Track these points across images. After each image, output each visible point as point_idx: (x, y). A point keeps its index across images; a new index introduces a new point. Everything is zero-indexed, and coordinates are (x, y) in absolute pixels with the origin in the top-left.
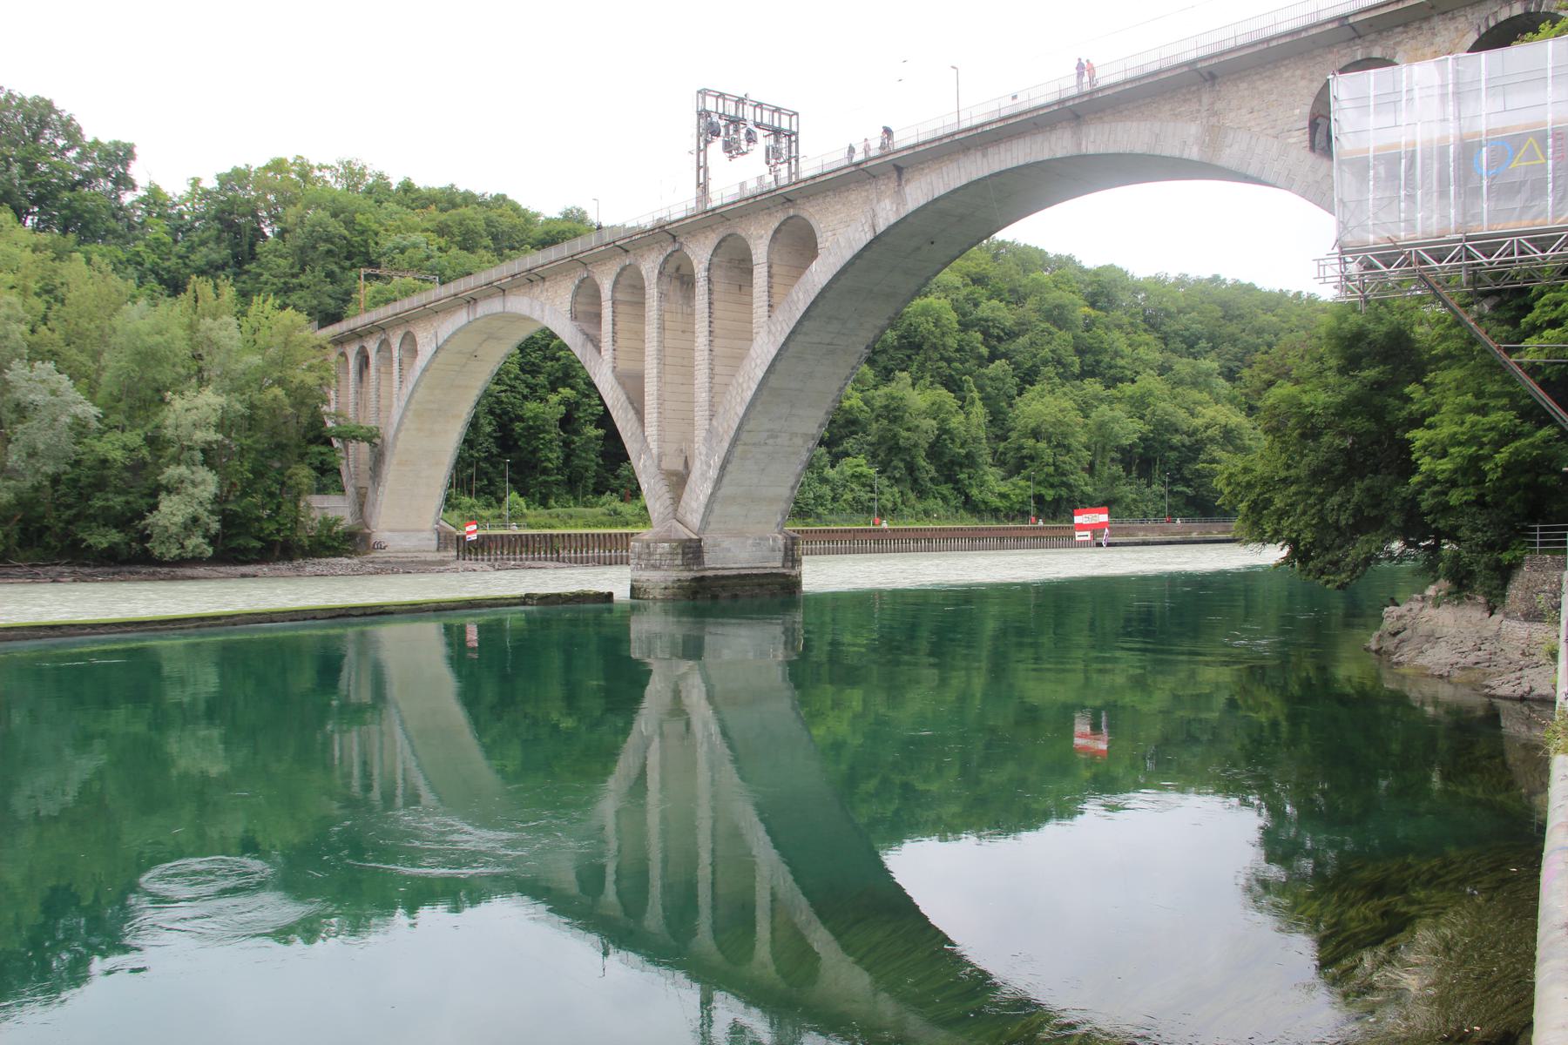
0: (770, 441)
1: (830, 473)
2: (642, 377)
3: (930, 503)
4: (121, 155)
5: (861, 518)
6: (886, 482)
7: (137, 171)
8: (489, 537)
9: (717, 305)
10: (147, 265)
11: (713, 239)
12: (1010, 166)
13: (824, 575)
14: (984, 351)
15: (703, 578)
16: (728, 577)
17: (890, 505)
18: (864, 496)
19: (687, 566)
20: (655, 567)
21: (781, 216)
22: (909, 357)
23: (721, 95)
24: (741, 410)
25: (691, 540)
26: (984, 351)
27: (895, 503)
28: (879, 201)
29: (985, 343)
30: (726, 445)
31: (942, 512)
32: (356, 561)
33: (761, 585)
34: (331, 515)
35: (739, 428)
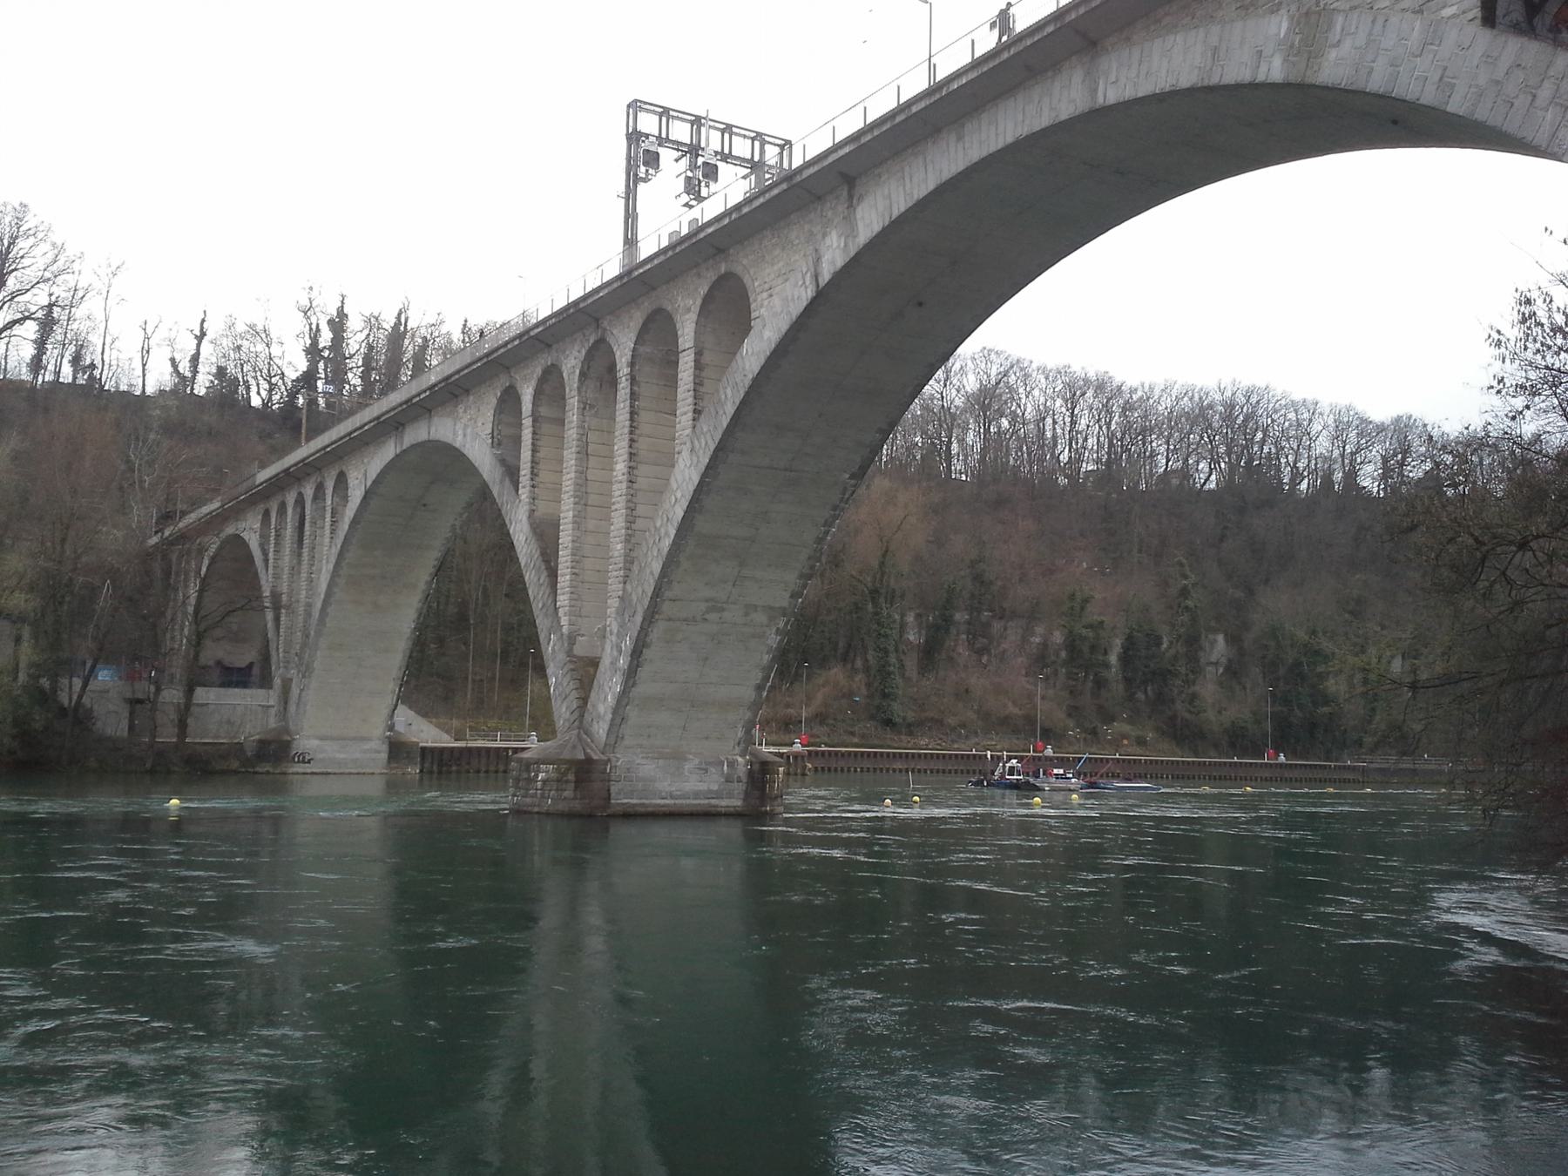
0: (713, 616)
8: (470, 749)
9: (644, 417)
11: (636, 319)
21: (711, 276)
23: (665, 113)
24: (657, 567)
28: (824, 235)
30: (639, 619)
35: (657, 593)
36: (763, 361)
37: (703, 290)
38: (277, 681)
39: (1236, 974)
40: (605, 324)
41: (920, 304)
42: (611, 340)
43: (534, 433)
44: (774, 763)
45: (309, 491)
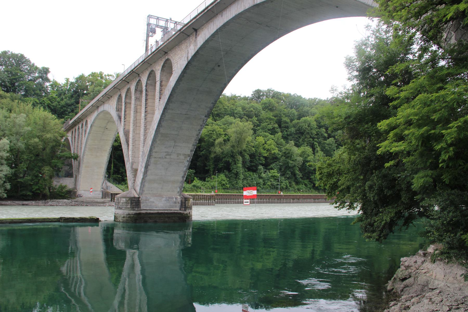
0: (167, 157)
1: (263, 175)
2: (129, 132)
3: (300, 186)
4: (46, 71)
5: (274, 191)
6: (283, 178)
7: (50, 76)
10: (46, 104)
12: (230, 18)
13: (201, 214)
14: (326, 135)
15: (140, 214)
16: (153, 214)
17: (284, 187)
18: (275, 183)
19: (132, 208)
20: (120, 208)
21: (164, 60)
22: (300, 137)
23: (158, 18)
24: (150, 143)
25: (135, 197)
26: (326, 135)
27: (287, 186)
28: (190, 46)
29: (327, 132)
30: (146, 158)
31: (304, 189)
32: (70, 201)
33: (169, 218)
34: (64, 185)
36: (175, 83)
37: (162, 64)
38: (74, 176)
39: (141, 160)
40: (140, 75)
41: (219, 66)
42: (141, 80)
43: (125, 107)
44: (188, 198)
45: (80, 126)
